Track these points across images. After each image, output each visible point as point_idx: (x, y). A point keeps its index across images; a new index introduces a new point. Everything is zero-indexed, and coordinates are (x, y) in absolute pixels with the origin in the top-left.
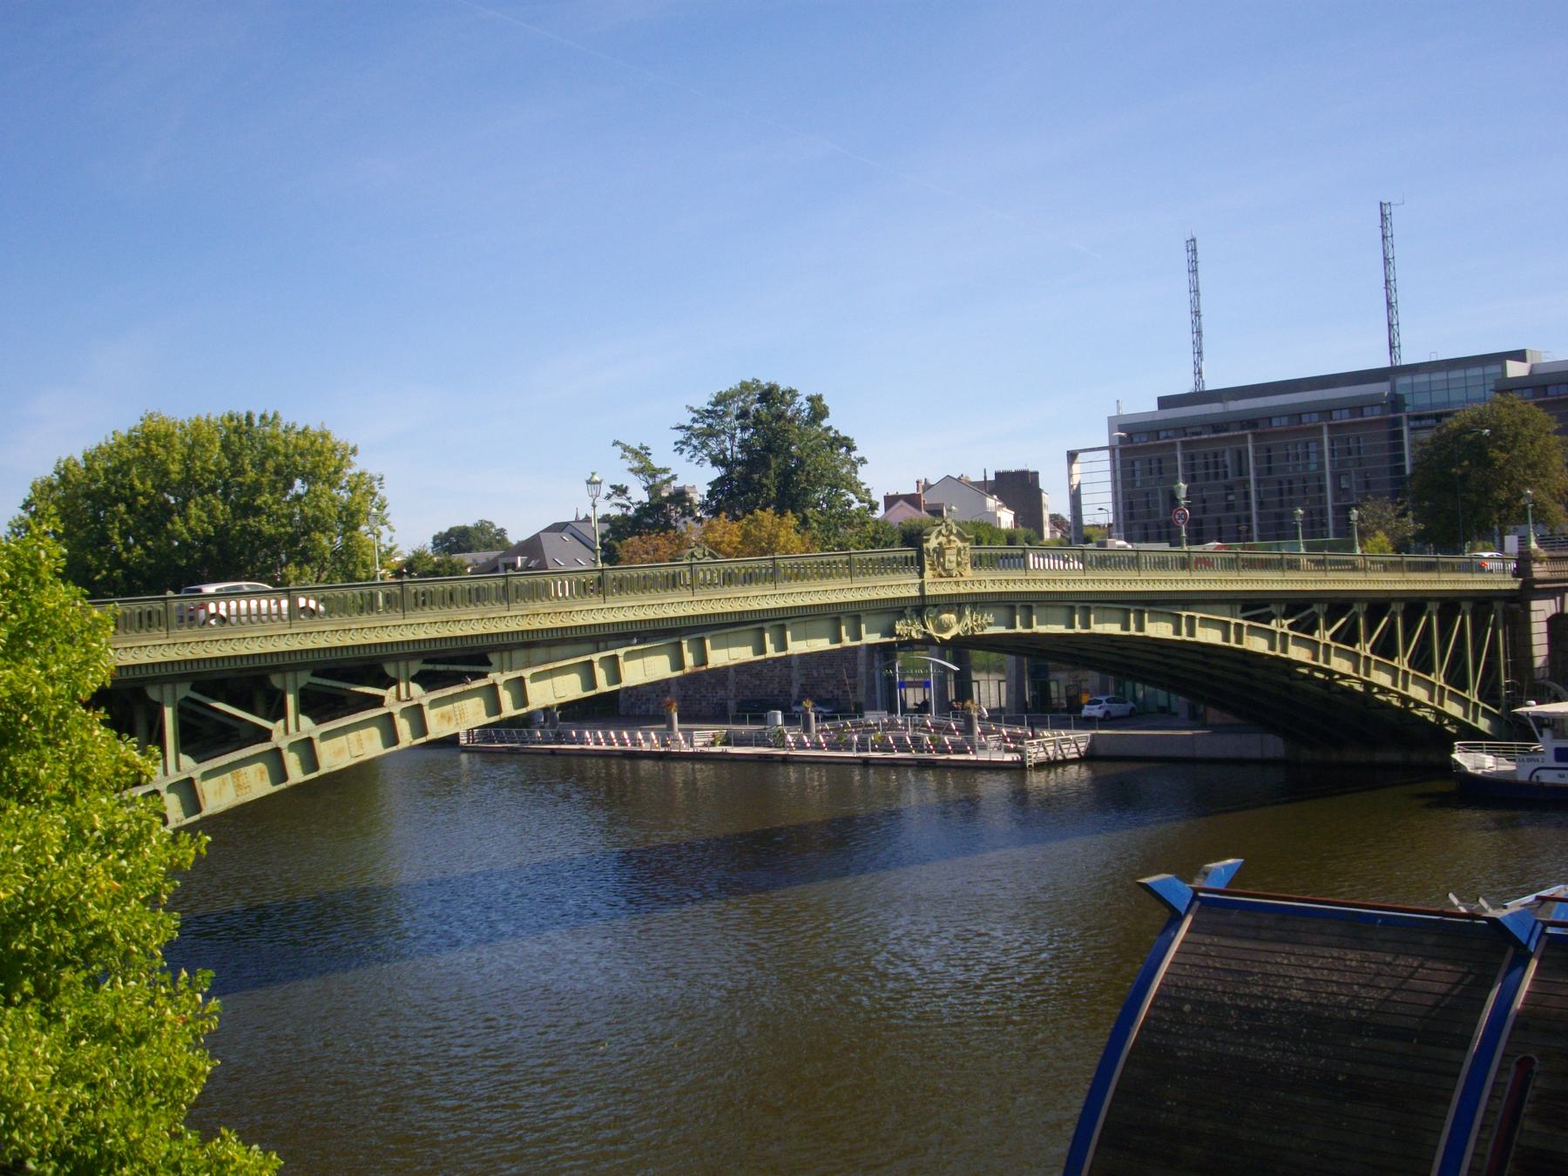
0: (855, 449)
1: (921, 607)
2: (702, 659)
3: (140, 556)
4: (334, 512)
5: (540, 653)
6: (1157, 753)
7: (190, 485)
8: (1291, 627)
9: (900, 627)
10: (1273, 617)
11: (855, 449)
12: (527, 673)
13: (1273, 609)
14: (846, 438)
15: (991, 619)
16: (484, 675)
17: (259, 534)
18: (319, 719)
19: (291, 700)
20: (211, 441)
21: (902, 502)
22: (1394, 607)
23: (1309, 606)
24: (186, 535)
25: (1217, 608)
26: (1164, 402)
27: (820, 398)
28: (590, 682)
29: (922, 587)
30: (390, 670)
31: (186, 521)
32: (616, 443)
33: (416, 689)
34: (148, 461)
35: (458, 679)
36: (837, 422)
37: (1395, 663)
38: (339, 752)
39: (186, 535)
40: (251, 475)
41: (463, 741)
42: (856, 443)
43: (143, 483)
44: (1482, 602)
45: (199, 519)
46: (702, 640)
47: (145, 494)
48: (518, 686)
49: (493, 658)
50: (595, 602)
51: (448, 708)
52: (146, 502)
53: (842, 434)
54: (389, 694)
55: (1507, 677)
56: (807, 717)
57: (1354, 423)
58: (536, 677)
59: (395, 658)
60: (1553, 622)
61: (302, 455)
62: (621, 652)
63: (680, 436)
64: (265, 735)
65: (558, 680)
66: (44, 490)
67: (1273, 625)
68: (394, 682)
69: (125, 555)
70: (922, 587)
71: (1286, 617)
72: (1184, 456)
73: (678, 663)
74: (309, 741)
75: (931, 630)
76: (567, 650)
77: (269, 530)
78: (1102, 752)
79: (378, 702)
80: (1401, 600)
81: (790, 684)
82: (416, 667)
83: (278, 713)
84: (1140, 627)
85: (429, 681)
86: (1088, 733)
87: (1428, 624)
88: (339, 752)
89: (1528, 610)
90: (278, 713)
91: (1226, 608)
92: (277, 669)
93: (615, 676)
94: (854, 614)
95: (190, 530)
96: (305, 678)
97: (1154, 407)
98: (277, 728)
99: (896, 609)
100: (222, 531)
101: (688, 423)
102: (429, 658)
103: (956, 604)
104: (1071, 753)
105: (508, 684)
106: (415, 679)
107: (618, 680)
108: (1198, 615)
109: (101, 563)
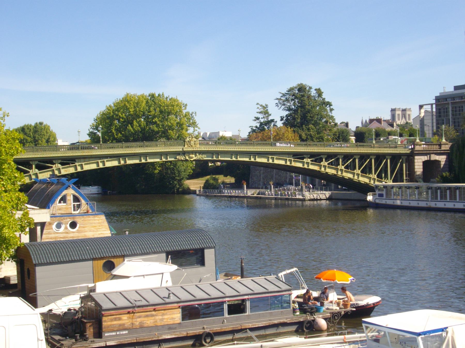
0: (332, 105)
1: (184, 153)
2: (125, 162)
3: (120, 137)
4: (175, 124)
5: (87, 160)
6: (343, 198)
7: (136, 116)
8: (312, 161)
9: (177, 157)
10: (305, 158)
11: (332, 105)
12: (83, 163)
13: (305, 156)
14: (328, 102)
15: (205, 156)
16: (74, 163)
17: (153, 131)
18: (39, 170)
19: (34, 166)
20: (142, 102)
21: (375, 121)
22: (371, 157)
23: (320, 156)
24: (132, 131)
25: (284, 155)
26: (456, 88)
27: (319, 89)
28: (98, 165)
29: (183, 149)
30: (54, 162)
31: (132, 127)
32: (258, 104)
33: (59, 165)
34: (126, 108)
35: (69, 164)
36: (327, 97)
37: (355, 171)
38: (43, 176)
39: (132, 131)
40: (153, 113)
41: (198, 193)
42: (332, 104)
43: (122, 114)
44: (395, 158)
45: (136, 126)
46: (125, 158)
47: (122, 118)
48: (81, 166)
49: (76, 160)
50: (71, 152)
51: (66, 169)
52: (123, 120)
53: (327, 100)
54: (54, 166)
55: (406, 177)
56: (271, 187)
57: (460, 102)
58: (85, 164)
59: (55, 159)
60: (438, 162)
61: (167, 106)
62: (105, 160)
63: (277, 101)
64: (29, 172)
65: (91, 165)
66: (302, 84)
67: (305, 160)
68: (55, 164)
69: (116, 136)
70: (183, 149)
71: (309, 158)
72: (453, 108)
73: (120, 163)
74: (37, 174)
75: (187, 158)
76: (93, 159)
77: (156, 129)
78: (334, 197)
79: (52, 167)
80: (374, 155)
81: (287, 178)
82: (60, 161)
83: (31, 168)
84: (255, 159)
85: (62, 164)
86: (330, 192)
87: (386, 163)
88: (43, 176)
89: (414, 159)
90: (31, 168)
91: (287, 156)
92: (31, 160)
93: (104, 165)
94: (166, 154)
95: (134, 129)
96: (37, 162)
97: (452, 89)
98: (31, 171)
99: (178, 153)
100: (143, 129)
101: (279, 98)
102: (62, 159)
103: (195, 152)
104: (324, 197)
105: (79, 165)
106: (59, 163)
107: (104, 165)
108: (275, 157)
109: (110, 138)
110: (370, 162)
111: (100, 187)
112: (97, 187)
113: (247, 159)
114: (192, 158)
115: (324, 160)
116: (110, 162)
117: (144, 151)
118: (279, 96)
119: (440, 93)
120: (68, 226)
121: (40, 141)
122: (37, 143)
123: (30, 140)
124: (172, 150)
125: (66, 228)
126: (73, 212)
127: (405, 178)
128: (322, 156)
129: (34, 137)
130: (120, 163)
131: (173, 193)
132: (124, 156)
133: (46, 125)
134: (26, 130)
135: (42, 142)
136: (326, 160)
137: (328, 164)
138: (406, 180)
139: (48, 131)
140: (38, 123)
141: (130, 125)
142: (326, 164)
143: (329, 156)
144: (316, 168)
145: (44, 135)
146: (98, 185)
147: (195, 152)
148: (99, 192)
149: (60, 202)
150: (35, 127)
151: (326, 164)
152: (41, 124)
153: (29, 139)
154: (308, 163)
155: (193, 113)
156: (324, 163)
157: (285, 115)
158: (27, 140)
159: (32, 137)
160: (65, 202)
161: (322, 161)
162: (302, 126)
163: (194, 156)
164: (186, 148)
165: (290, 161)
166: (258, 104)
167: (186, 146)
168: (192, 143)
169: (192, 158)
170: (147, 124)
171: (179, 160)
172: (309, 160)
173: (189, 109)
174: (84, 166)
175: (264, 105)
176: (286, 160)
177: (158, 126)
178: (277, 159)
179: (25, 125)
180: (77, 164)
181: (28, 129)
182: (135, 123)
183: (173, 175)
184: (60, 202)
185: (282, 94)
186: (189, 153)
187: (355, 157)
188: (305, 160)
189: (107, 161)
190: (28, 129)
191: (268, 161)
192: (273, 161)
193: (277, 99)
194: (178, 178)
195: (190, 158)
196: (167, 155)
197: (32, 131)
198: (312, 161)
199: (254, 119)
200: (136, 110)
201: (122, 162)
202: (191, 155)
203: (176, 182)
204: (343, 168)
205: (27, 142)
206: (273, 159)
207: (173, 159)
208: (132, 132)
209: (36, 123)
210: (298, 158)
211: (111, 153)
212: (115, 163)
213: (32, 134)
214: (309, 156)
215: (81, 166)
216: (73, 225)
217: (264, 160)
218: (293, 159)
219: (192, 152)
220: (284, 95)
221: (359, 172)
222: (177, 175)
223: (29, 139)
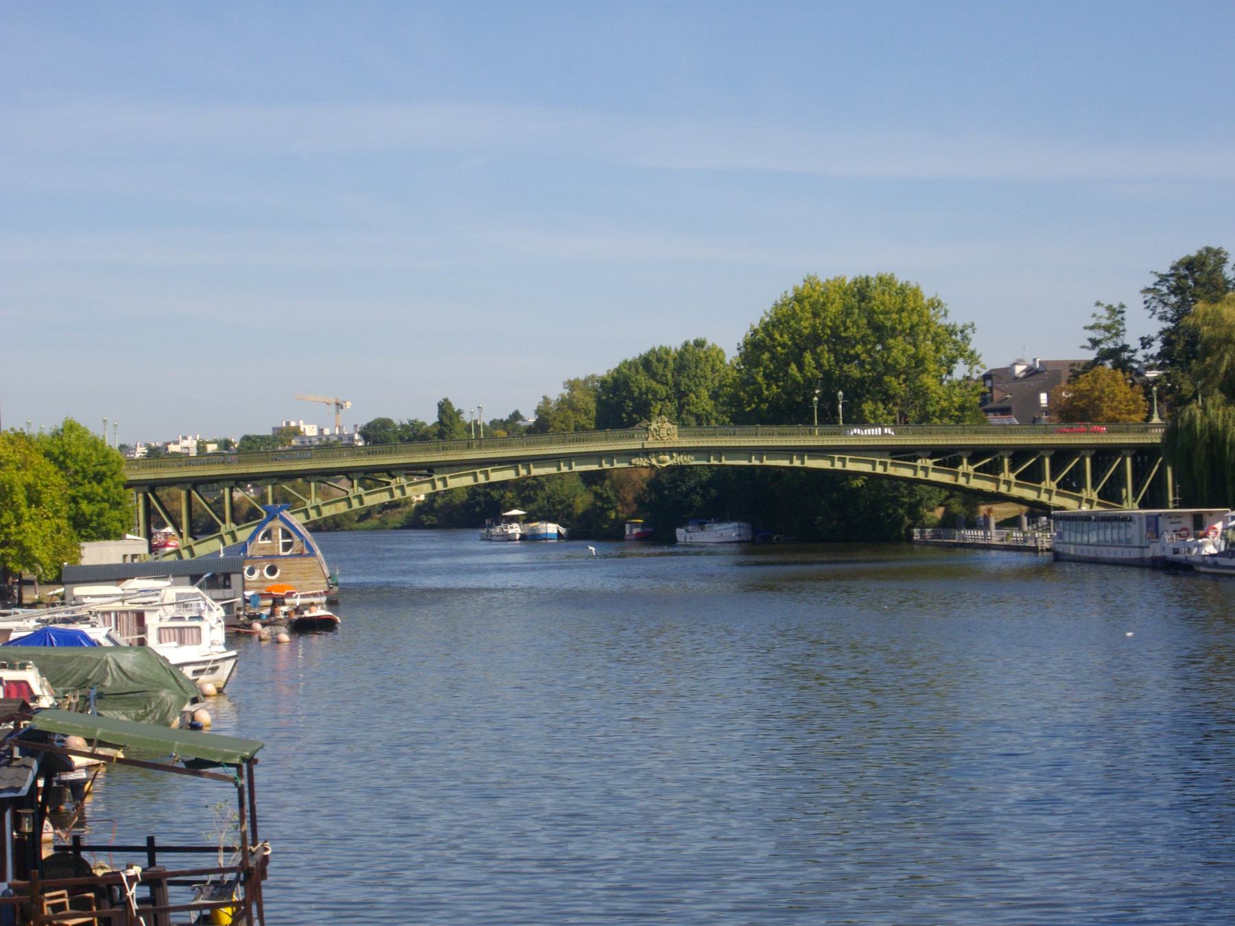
1: (646, 453)
2: (529, 472)
13: (919, 454)
22: (1124, 452)
28: (476, 480)
32: (1098, 304)
47: (784, 346)
48: (444, 480)
54: (393, 481)
55: (1174, 495)
67: (919, 463)
71: (930, 458)
73: (517, 473)
75: (654, 462)
95: (804, 376)
103: (670, 451)
110: (1081, 464)
111: (745, 524)
112: (735, 524)
113: (786, 463)
114: (664, 462)
115: (965, 461)
116: (500, 473)
117: (607, 448)
118: (1150, 281)
119: (274, 429)
120: (265, 571)
121: (692, 395)
122: (684, 400)
123: (664, 394)
124: (621, 448)
125: (262, 574)
126: (282, 553)
127: (1171, 498)
128: (960, 454)
129: (677, 385)
130: (517, 473)
131: (899, 539)
132: (526, 461)
133: (714, 347)
134: (655, 363)
135: (697, 397)
136: (971, 463)
137: (976, 470)
138: (1174, 502)
139: (718, 365)
140: (692, 343)
141: (793, 366)
142: (971, 469)
143: (976, 454)
144: (946, 479)
145: (705, 377)
146: (733, 520)
147: (670, 451)
148: (742, 538)
149: (263, 539)
150: (681, 355)
151: (971, 469)
152: (699, 344)
153: (662, 390)
154: (925, 469)
155: (965, 327)
156: (965, 467)
157: (1154, 334)
158: (655, 393)
159: (670, 382)
160: (270, 538)
161: (961, 463)
162: (1188, 363)
163: (667, 458)
164: (651, 444)
165: (884, 464)
166: (1098, 304)
167: (651, 439)
168: (664, 432)
169: (664, 462)
170: (837, 362)
171: (636, 466)
172: (929, 463)
173: (956, 318)
174: (449, 481)
175: (1116, 306)
176: (873, 463)
177: (862, 364)
178: (851, 460)
179: (653, 351)
180: (436, 477)
181: (659, 360)
182: (808, 357)
183: (896, 493)
184: (263, 539)
185: (1160, 276)
186: (657, 452)
187: (1042, 453)
188: (919, 461)
189: (493, 471)
190: (659, 360)
191: (833, 465)
192: (844, 465)
193: (1148, 290)
194: (906, 500)
195: (659, 461)
196: (570, 462)
197: (671, 365)
198: (935, 464)
199: (1089, 344)
200: (814, 327)
201: (523, 472)
202: (661, 457)
203: (901, 511)
204: (1012, 477)
205: (656, 399)
206: (486, 474)
207: (626, 465)
208: (798, 383)
209: (687, 344)
210: (905, 459)
211: (499, 455)
212: (508, 475)
213: (669, 376)
214: (929, 454)
215: (444, 480)
216: (272, 571)
217: (823, 464)
218: (889, 461)
219: (664, 451)
220: (1163, 279)
221: (1053, 486)
222: (906, 492)
223: (662, 390)
